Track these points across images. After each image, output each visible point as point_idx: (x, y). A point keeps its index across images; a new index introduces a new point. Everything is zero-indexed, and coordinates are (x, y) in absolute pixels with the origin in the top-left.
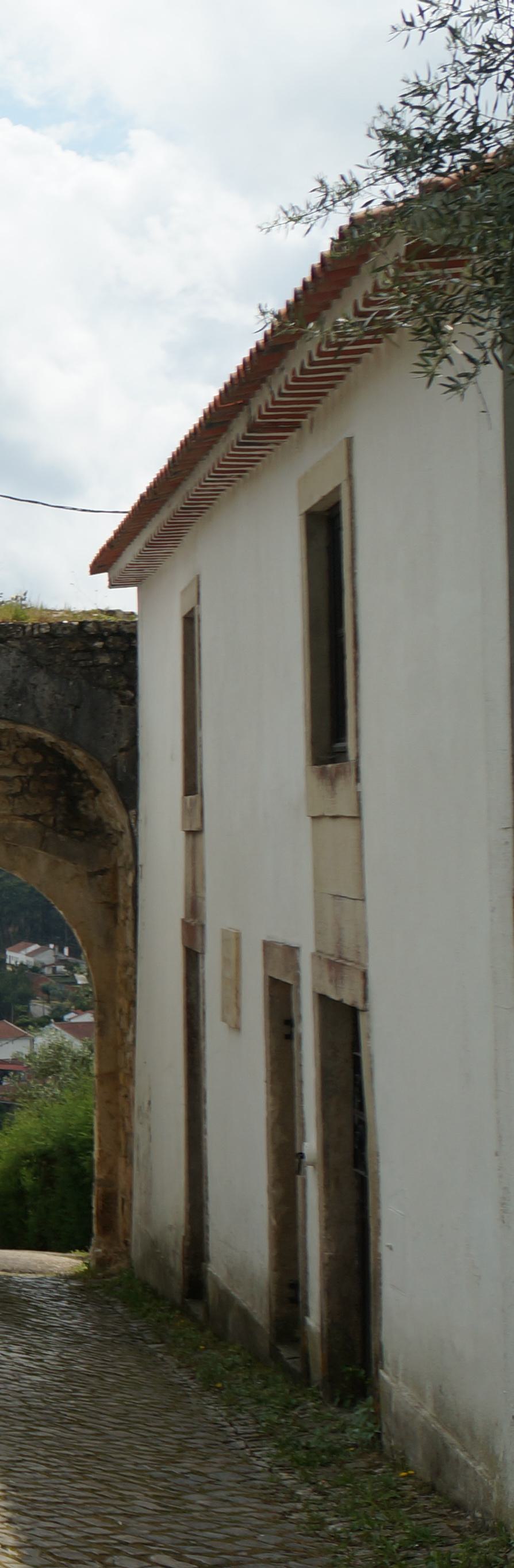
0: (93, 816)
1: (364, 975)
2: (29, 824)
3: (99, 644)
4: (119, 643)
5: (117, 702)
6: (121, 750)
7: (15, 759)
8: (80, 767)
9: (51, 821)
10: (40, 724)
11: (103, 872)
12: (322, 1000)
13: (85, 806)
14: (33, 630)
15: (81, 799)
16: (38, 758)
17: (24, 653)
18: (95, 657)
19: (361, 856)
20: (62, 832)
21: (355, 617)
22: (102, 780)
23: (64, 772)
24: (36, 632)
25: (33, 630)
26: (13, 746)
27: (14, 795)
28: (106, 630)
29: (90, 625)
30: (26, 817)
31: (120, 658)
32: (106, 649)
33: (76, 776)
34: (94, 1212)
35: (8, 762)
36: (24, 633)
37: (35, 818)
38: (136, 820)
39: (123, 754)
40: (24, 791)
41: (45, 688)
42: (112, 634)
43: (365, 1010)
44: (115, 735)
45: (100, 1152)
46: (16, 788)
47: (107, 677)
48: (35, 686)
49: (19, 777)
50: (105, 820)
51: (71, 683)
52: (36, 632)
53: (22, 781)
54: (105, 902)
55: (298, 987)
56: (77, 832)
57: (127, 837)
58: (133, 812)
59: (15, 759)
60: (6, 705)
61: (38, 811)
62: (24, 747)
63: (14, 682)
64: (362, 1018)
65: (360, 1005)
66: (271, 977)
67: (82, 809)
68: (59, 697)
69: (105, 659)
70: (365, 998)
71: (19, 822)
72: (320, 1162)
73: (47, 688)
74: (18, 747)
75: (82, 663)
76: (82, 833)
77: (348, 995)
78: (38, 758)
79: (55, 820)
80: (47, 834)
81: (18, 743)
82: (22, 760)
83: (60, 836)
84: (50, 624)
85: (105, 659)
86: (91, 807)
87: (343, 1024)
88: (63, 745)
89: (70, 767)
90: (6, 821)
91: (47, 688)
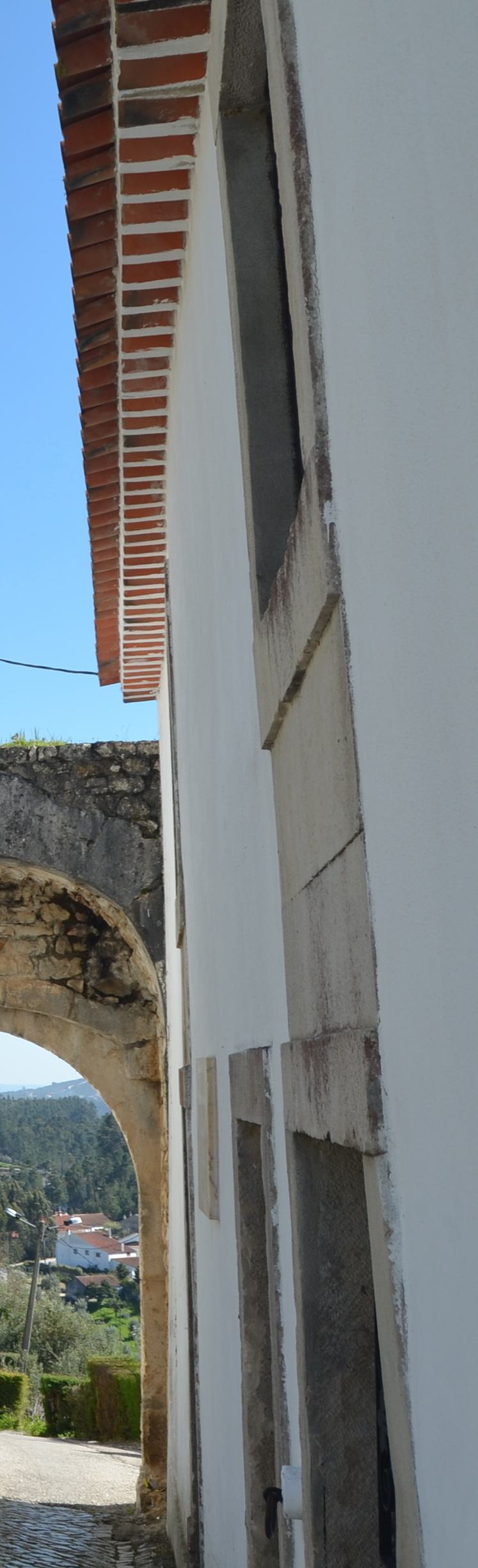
0: (129, 981)
1: (371, 1047)
2: (56, 989)
3: (115, 768)
4: (137, 767)
5: (137, 834)
6: (144, 891)
7: (39, 917)
8: (110, 923)
9: (81, 986)
10: (47, 862)
11: (142, 1043)
12: (300, 1139)
13: (120, 969)
14: (37, 753)
15: (115, 961)
16: (65, 915)
17: (28, 781)
18: (113, 788)
20: (93, 998)
21: (291, 70)
22: (130, 933)
23: (94, 931)
24: (41, 756)
25: (37, 753)
26: (37, 903)
27: (39, 957)
28: (122, 751)
29: (105, 747)
30: (52, 981)
31: (141, 784)
32: (123, 773)
33: (108, 935)
34: (142, 1436)
35: (31, 919)
36: (28, 757)
37: (62, 982)
38: (164, 973)
39: (147, 895)
40: (50, 952)
41: (54, 819)
42: (129, 756)
43: (380, 1153)
44: (137, 874)
45: (147, 1368)
47: (125, 807)
48: (41, 818)
49: (45, 936)
50: (142, 985)
51: (83, 814)
52: (41, 756)
53: (47, 942)
54: (143, 1079)
56: (111, 999)
58: (160, 963)
59: (39, 917)
60: (8, 841)
61: (66, 975)
62: (49, 903)
63: (17, 813)
64: (372, 1172)
65: (363, 1141)
66: (239, 1121)
67: (116, 972)
68: (70, 830)
69: (122, 785)
70: (375, 1116)
71: (45, 987)
72: (309, 1515)
73: (55, 819)
74: (42, 903)
75: (96, 791)
76: (117, 1000)
77: (338, 1122)
78: (65, 915)
79: (85, 985)
80: (76, 1000)
81: (43, 899)
82: (47, 917)
83: (91, 1003)
84: (58, 747)
85: (122, 785)
86: (126, 970)
88: (85, 892)
89: (98, 922)
90: (30, 986)
91: (55, 819)
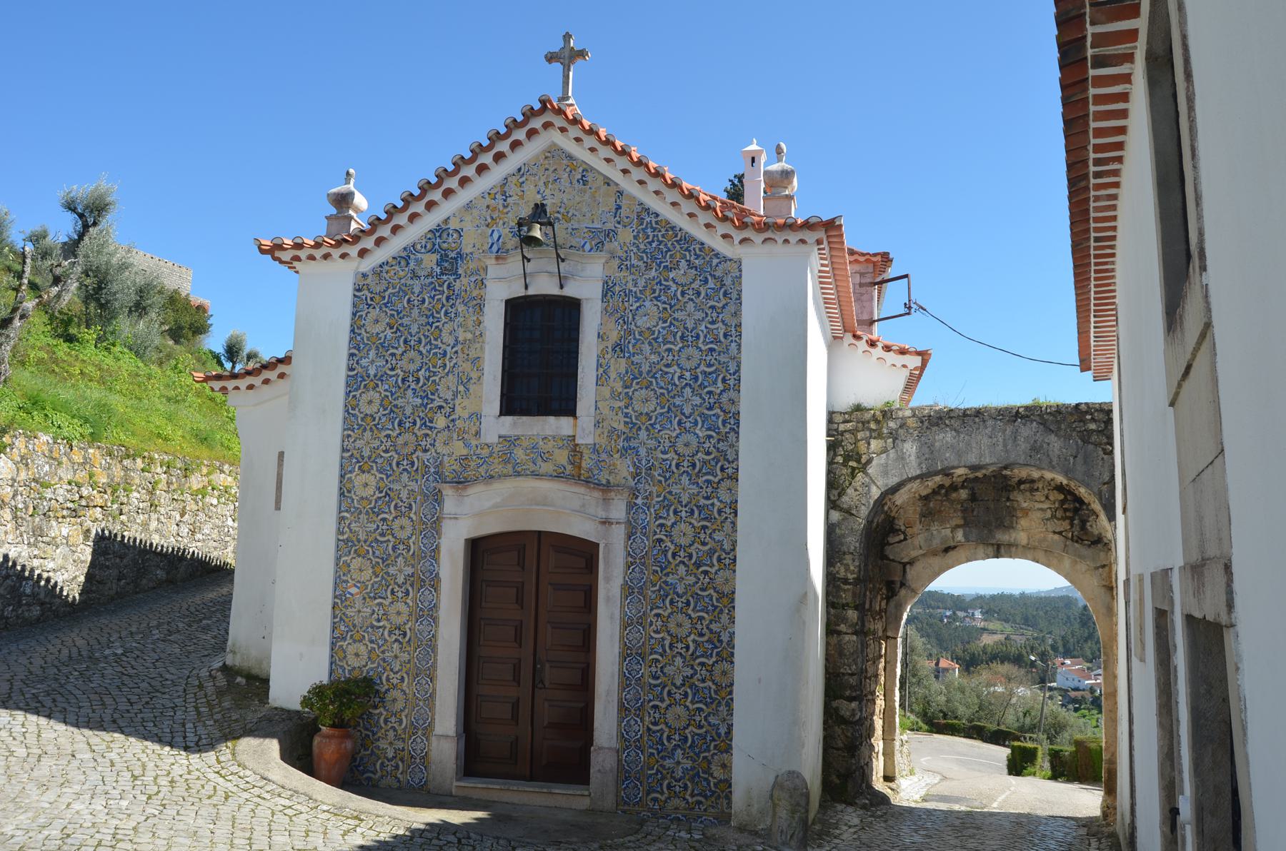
1: (1228, 568)
2: (1056, 537)
3: (1089, 417)
7: (1047, 498)
10: (1052, 468)
11: (1104, 566)
12: (1189, 619)
19: (1215, 381)
22: (1096, 506)
32: (1093, 420)
37: (1060, 533)
40: (1053, 516)
41: (1055, 444)
42: (1097, 410)
46: (1049, 514)
47: (1094, 438)
55: (1173, 613)
57: (945, 437)
59: (1047, 498)
64: (1228, 636)
65: (1224, 619)
69: (1093, 426)
70: (1230, 606)
72: (1194, 822)
77: (1210, 609)
78: (1062, 497)
82: (1051, 498)
85: (1093, 426)
87: (1210, 639)
88: (1072, 484)
89: (1079, 500)
